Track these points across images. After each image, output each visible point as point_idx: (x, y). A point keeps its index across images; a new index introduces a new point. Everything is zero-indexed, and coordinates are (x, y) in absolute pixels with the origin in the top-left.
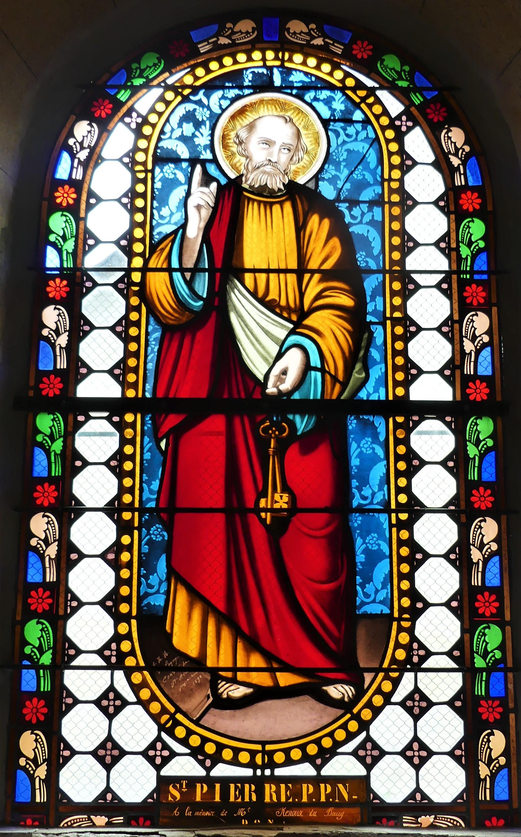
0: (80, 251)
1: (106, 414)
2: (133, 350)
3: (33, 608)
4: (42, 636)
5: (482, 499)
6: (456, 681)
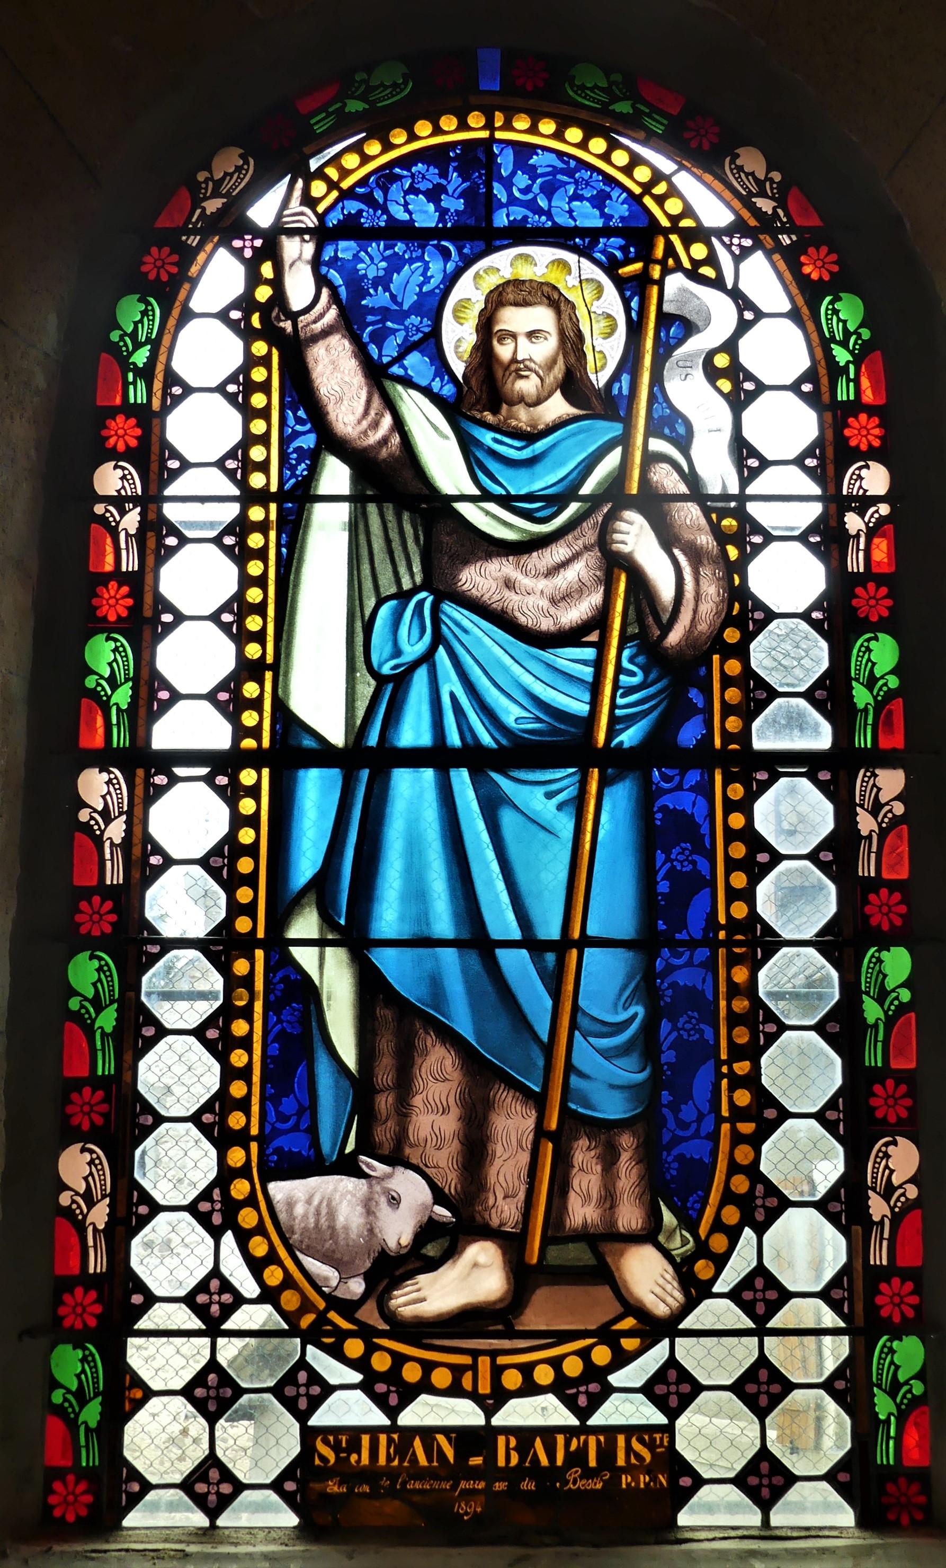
0: (142, 711)
1: (204, 771)
2: (260, 433)
3: (83, 930)
4: (100, 980)
5: (864, 431)
6: (834, 1249)
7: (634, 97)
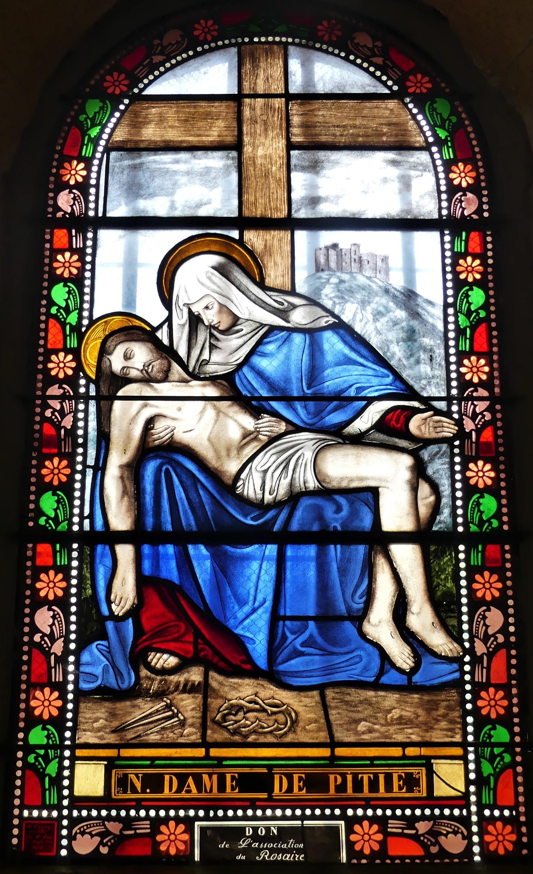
7: (451, 134)
